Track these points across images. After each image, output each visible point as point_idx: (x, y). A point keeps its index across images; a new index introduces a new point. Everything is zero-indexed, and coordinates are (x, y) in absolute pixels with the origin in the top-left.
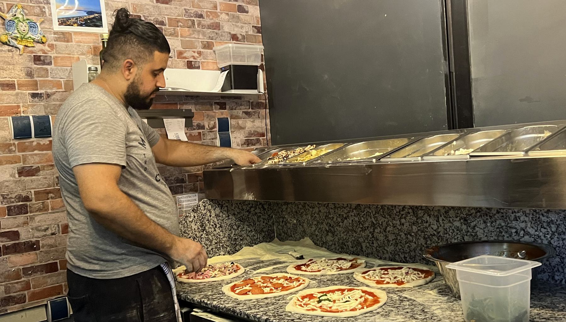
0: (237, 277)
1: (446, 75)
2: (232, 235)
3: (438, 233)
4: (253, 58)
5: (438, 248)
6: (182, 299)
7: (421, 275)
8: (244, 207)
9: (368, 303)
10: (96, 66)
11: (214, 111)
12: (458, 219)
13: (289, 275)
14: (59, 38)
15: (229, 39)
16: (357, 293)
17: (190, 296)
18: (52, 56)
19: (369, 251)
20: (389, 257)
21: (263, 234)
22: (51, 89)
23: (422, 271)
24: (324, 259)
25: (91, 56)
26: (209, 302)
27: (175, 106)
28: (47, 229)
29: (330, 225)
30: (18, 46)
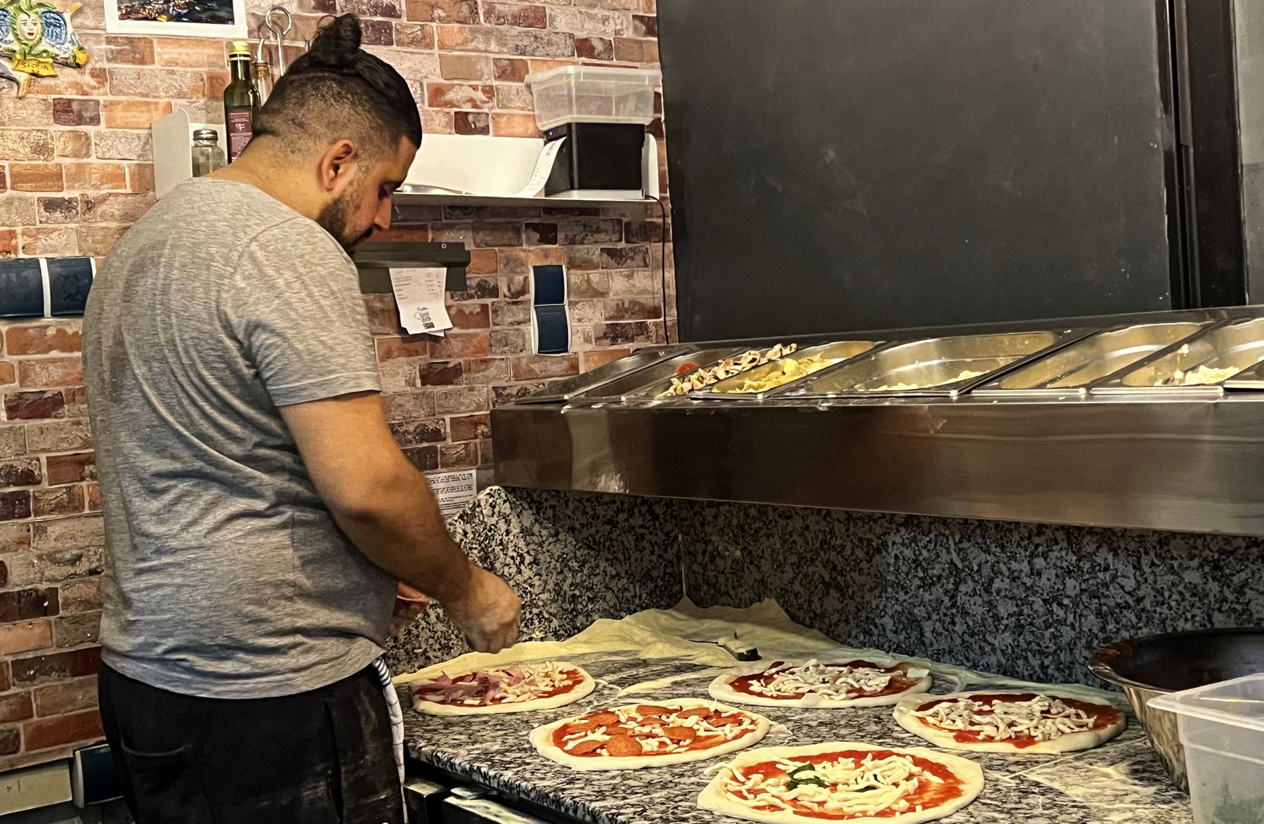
0: (575, 703)
1: (1168, 156)
2: (566, 587)
3: (1139, 600)
4: (631, 105)
5: (1136, 645)
6: (423, 759)
7: (1085, 719)
8: (600, 511)
9: (927, 797)
10: (213, 127)
11: (525, 247)
12: (1195, 563)
13: (713, 706)
14: (119, 52)
15: (568, 51)
16: (899, 766)
17: (445, 752)
18: (102, 99)
19: (944, 645)
20: (1000, 665)
21: (651, 585)
22: (96, 187)
23: (1090, 709)
24: (813, 661)
25: (202, 101)
26: (492, 773)
27: (420, 233)
28: (79, 557)
29: (834, 568)
30: (15, 75)
